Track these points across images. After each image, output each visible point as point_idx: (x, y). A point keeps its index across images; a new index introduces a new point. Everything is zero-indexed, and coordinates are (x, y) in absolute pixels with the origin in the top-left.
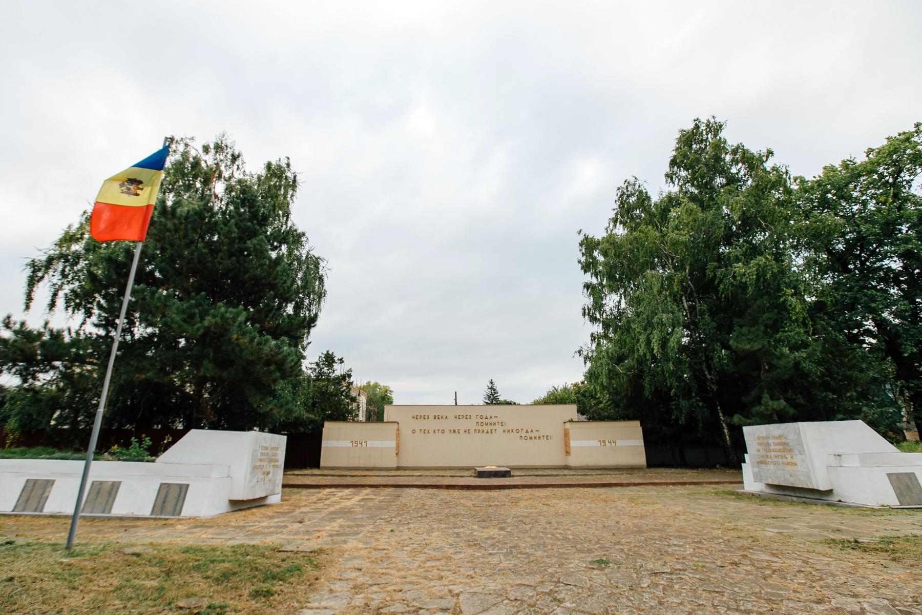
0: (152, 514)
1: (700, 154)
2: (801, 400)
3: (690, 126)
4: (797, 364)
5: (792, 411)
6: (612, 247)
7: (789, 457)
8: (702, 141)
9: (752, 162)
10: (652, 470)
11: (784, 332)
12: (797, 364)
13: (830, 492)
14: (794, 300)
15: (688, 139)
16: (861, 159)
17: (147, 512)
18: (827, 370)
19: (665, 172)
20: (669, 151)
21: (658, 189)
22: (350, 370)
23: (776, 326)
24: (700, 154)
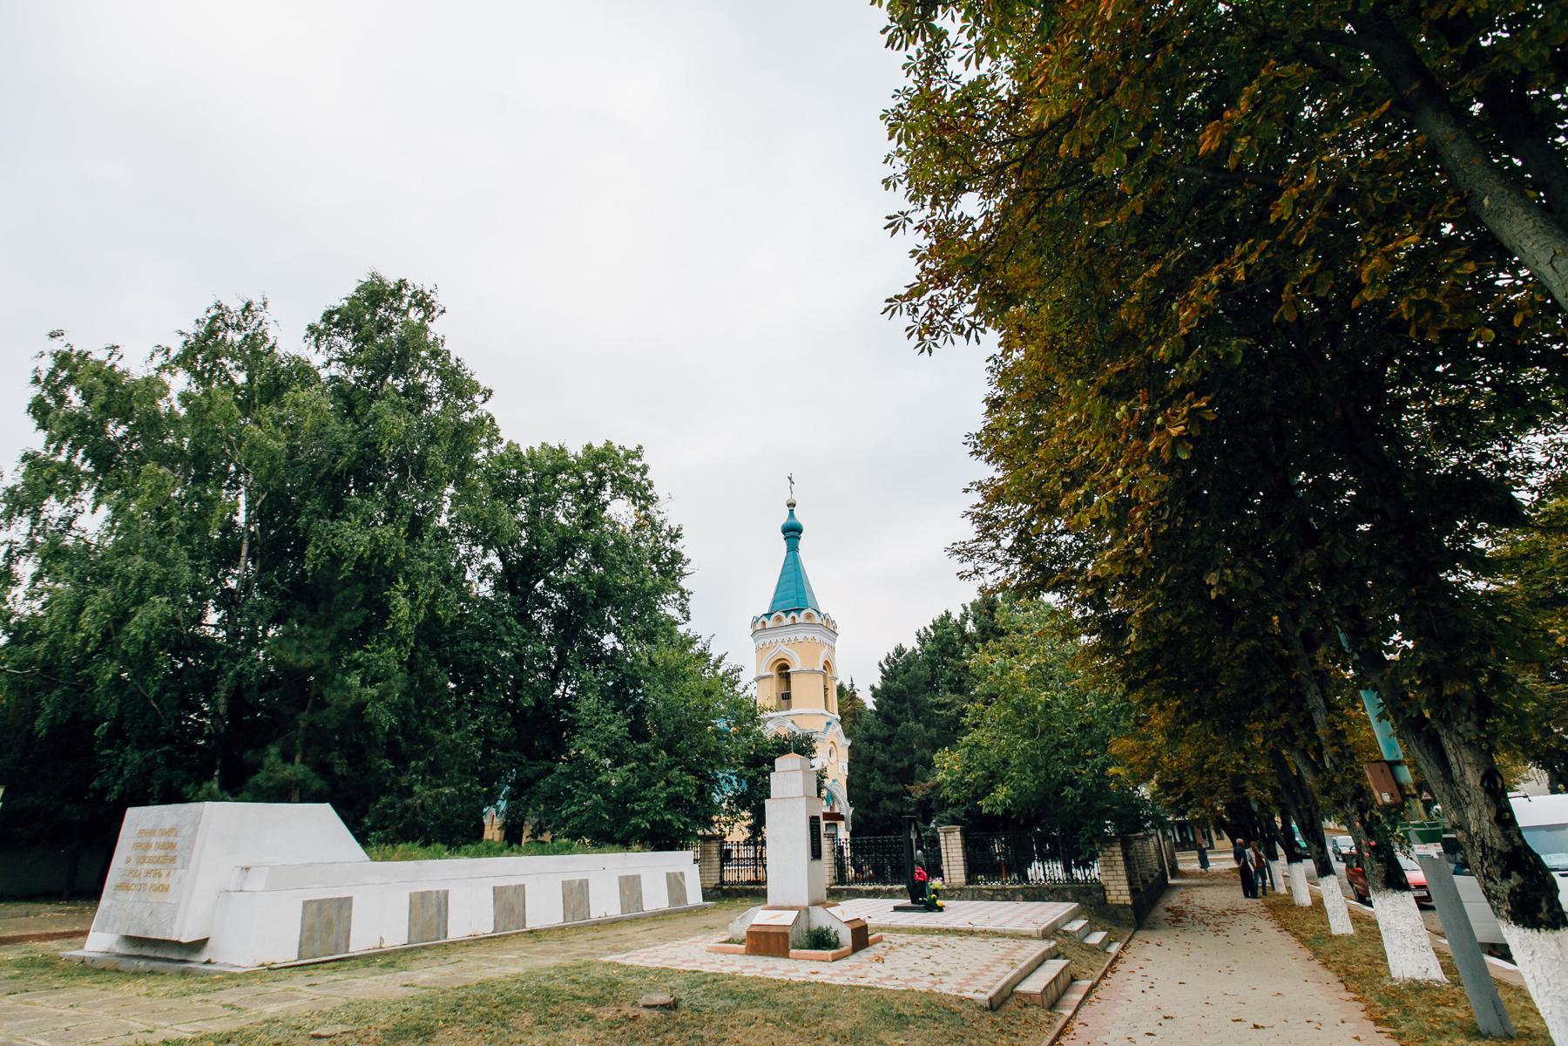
0: (300, 958)
1: (381, 324)
2: (341, 768)
3: (391, 279)
4: (360, 707)
5: (317, 784)
6: (104, 389)
7: (164, 873)
8: (397, 310)
9: (458, 385)
10: (945, 869)
11: (367, 650)
12: (360, 707)
13: (199, 945)
14: (403, 600)
15: (376, 294)
16: (575, 449)
17: (488, 929)
18: (404, 724)
19: (310, 322)
20: (339, 293)
21: (288, 339)
22: (640, 447)
23: (359, 636)
24: (381, 324)
